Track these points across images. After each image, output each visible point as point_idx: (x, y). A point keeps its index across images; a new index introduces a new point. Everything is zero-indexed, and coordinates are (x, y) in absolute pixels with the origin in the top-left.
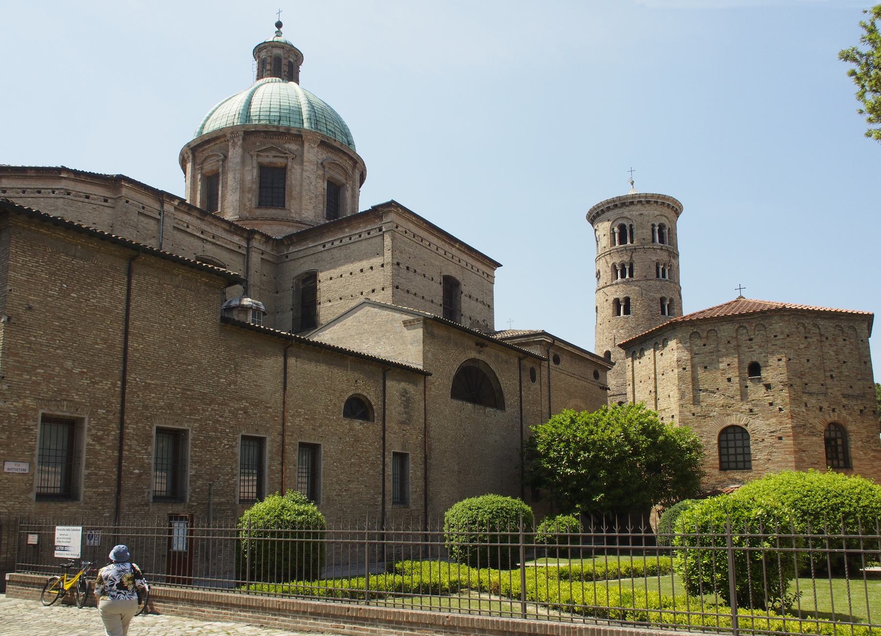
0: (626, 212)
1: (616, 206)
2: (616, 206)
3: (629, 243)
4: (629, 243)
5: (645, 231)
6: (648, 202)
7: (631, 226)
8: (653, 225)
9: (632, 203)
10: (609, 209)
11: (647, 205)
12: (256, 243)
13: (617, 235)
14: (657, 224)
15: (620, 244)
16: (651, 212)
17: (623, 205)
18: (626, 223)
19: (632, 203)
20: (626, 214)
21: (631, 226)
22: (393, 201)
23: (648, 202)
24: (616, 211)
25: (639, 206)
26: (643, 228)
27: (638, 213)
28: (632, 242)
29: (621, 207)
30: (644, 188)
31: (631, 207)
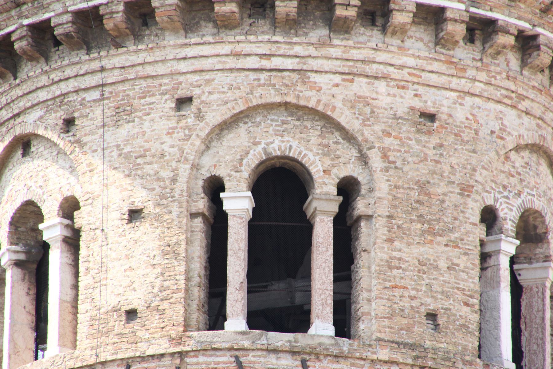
3: (322, 326)
4: (322, 326)
20: (327, 90)
21: (348, 189)
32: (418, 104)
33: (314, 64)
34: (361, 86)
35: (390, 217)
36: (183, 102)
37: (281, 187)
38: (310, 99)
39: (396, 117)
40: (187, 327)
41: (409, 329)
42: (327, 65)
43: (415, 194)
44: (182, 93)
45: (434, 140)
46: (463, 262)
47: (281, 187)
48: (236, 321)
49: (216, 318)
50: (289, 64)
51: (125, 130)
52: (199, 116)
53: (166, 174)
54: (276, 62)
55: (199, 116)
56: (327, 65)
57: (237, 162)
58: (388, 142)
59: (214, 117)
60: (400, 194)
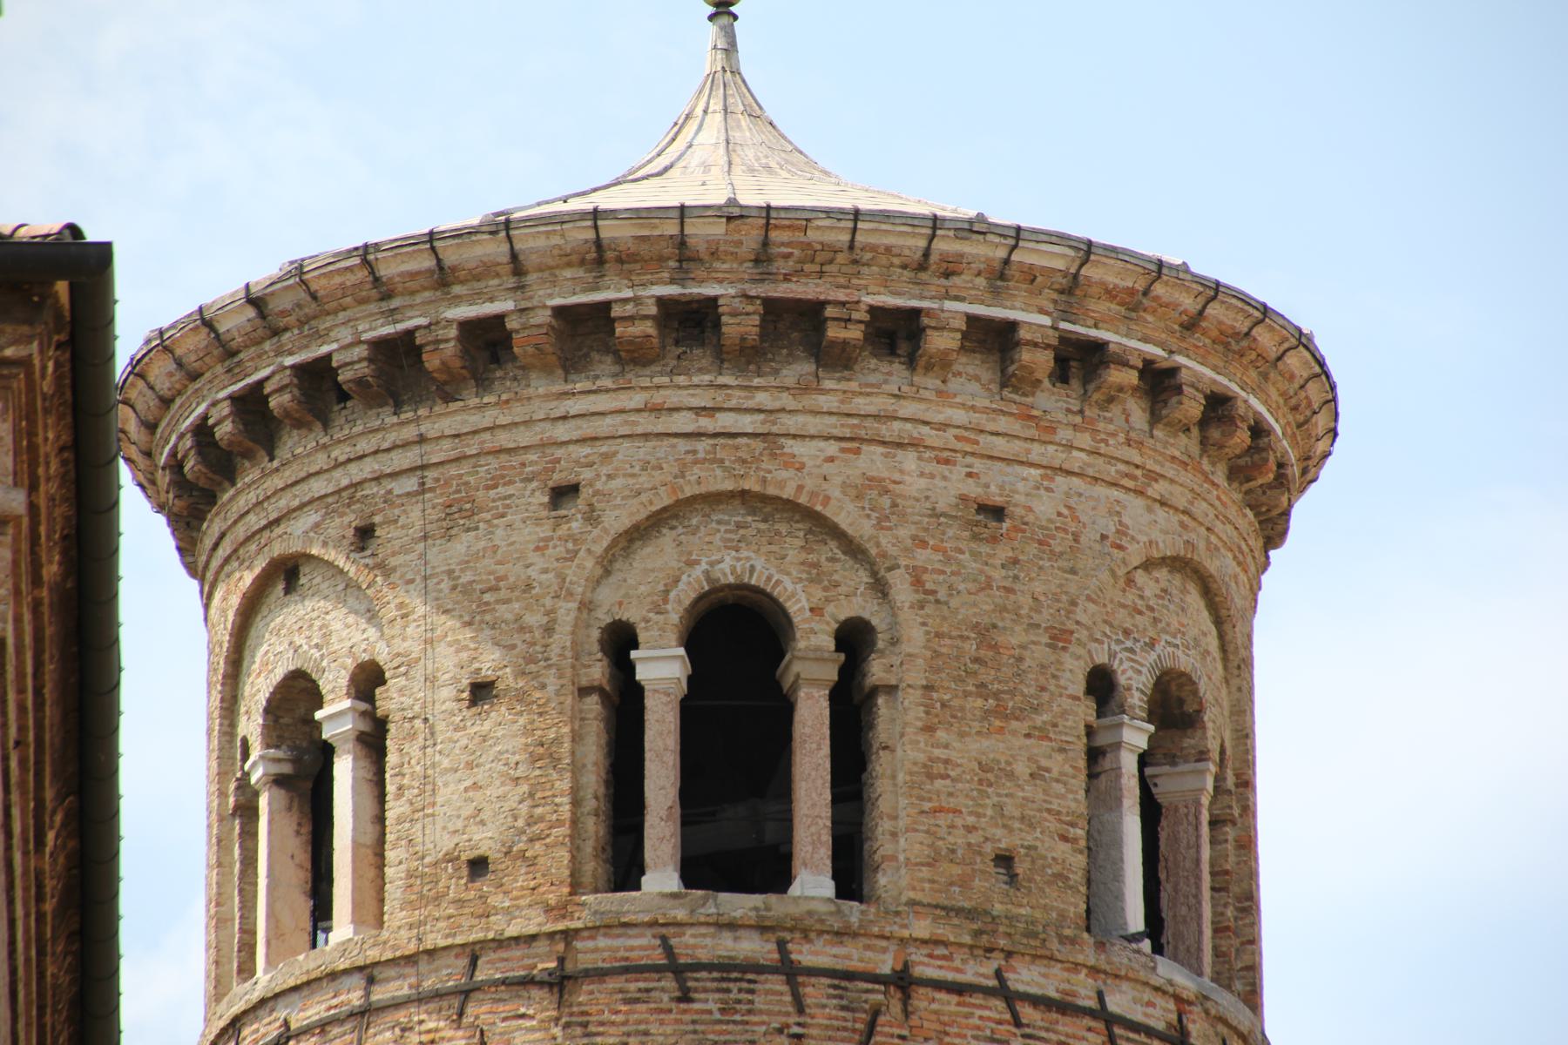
0: (811, 430)
1: (691, 323)
2: (691, 323)
3: (813, 882)
4: (813, 882)
5: (1011, 747)
6: (1080, 361)
7: (854, 640)
8: (1101, 685)
9: (897, 334)
10: (584, 334)
11: (1051, 401)
12: (815, 992)
13: (46, 609)
14: (1135, 682)
15: (700, 871)
16: (1097, 507)
17: (796, 328)
18: (796, 598)
19: (897, 334)
20: (815, 468)
21: (854, 640)
22: (981, 218)
23: (1080, 361)
24: (689, 391)
25: (968, 394)
26: (1001, 713)
27: (952, 486)
28: (851, 875)
29: (750, 357)
30: (881, 131)
31: (879, 387)
32: (973, 490)
33: (790, 423)
34: (873, 460)
35: (928, 688)
36: (563, 494)
37: (736, 637)
38: (784, 483)
39: (935, 514)
40: (576, 887)
41: (964, 882)
42: (814, 424)
43: (971, 647)
44: (558, 478)
45: (1003, 552)
46: (1056, 764)
47: (736, 637)
48: (661, 878)
49: (625, 870)
50: (747, 423)
51: (461, 545)
52: (592, 517)
53: (535, 619)
54: (725, 421)
55: (592, 517)
56: (814, 424)
57: (658, 596)
58: (923, 556)
59: (618, 519)
60: (945, 647)
